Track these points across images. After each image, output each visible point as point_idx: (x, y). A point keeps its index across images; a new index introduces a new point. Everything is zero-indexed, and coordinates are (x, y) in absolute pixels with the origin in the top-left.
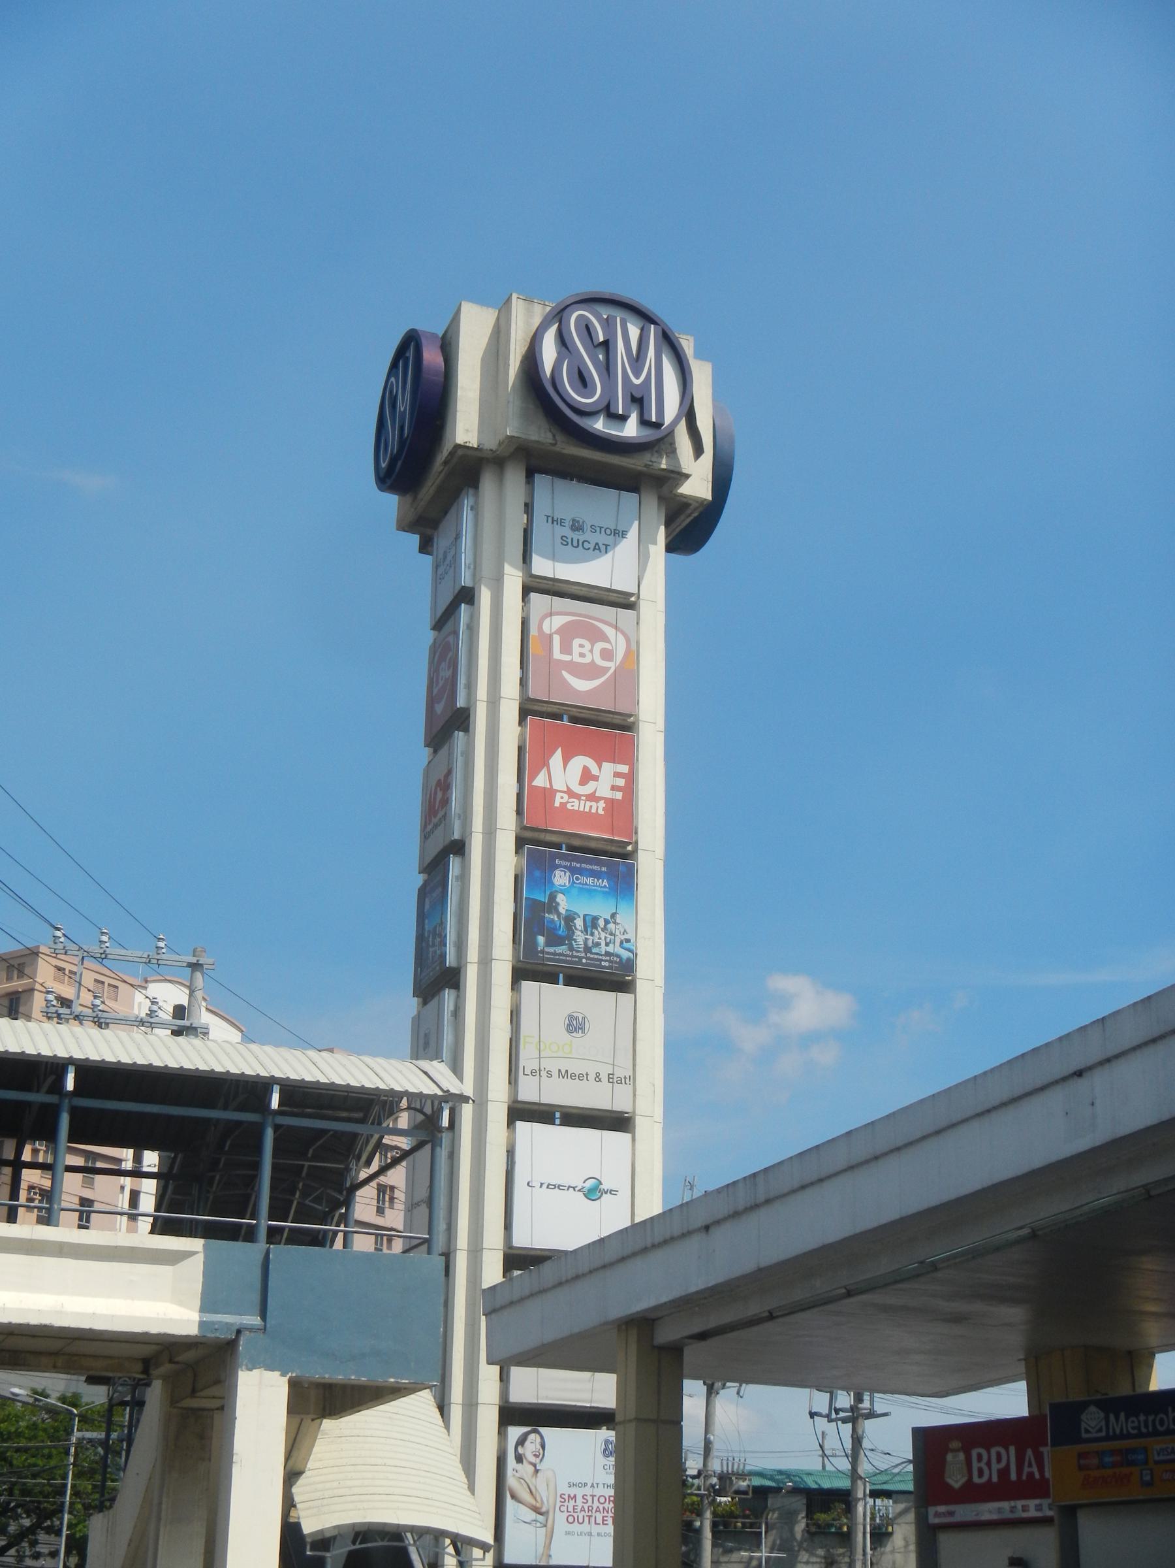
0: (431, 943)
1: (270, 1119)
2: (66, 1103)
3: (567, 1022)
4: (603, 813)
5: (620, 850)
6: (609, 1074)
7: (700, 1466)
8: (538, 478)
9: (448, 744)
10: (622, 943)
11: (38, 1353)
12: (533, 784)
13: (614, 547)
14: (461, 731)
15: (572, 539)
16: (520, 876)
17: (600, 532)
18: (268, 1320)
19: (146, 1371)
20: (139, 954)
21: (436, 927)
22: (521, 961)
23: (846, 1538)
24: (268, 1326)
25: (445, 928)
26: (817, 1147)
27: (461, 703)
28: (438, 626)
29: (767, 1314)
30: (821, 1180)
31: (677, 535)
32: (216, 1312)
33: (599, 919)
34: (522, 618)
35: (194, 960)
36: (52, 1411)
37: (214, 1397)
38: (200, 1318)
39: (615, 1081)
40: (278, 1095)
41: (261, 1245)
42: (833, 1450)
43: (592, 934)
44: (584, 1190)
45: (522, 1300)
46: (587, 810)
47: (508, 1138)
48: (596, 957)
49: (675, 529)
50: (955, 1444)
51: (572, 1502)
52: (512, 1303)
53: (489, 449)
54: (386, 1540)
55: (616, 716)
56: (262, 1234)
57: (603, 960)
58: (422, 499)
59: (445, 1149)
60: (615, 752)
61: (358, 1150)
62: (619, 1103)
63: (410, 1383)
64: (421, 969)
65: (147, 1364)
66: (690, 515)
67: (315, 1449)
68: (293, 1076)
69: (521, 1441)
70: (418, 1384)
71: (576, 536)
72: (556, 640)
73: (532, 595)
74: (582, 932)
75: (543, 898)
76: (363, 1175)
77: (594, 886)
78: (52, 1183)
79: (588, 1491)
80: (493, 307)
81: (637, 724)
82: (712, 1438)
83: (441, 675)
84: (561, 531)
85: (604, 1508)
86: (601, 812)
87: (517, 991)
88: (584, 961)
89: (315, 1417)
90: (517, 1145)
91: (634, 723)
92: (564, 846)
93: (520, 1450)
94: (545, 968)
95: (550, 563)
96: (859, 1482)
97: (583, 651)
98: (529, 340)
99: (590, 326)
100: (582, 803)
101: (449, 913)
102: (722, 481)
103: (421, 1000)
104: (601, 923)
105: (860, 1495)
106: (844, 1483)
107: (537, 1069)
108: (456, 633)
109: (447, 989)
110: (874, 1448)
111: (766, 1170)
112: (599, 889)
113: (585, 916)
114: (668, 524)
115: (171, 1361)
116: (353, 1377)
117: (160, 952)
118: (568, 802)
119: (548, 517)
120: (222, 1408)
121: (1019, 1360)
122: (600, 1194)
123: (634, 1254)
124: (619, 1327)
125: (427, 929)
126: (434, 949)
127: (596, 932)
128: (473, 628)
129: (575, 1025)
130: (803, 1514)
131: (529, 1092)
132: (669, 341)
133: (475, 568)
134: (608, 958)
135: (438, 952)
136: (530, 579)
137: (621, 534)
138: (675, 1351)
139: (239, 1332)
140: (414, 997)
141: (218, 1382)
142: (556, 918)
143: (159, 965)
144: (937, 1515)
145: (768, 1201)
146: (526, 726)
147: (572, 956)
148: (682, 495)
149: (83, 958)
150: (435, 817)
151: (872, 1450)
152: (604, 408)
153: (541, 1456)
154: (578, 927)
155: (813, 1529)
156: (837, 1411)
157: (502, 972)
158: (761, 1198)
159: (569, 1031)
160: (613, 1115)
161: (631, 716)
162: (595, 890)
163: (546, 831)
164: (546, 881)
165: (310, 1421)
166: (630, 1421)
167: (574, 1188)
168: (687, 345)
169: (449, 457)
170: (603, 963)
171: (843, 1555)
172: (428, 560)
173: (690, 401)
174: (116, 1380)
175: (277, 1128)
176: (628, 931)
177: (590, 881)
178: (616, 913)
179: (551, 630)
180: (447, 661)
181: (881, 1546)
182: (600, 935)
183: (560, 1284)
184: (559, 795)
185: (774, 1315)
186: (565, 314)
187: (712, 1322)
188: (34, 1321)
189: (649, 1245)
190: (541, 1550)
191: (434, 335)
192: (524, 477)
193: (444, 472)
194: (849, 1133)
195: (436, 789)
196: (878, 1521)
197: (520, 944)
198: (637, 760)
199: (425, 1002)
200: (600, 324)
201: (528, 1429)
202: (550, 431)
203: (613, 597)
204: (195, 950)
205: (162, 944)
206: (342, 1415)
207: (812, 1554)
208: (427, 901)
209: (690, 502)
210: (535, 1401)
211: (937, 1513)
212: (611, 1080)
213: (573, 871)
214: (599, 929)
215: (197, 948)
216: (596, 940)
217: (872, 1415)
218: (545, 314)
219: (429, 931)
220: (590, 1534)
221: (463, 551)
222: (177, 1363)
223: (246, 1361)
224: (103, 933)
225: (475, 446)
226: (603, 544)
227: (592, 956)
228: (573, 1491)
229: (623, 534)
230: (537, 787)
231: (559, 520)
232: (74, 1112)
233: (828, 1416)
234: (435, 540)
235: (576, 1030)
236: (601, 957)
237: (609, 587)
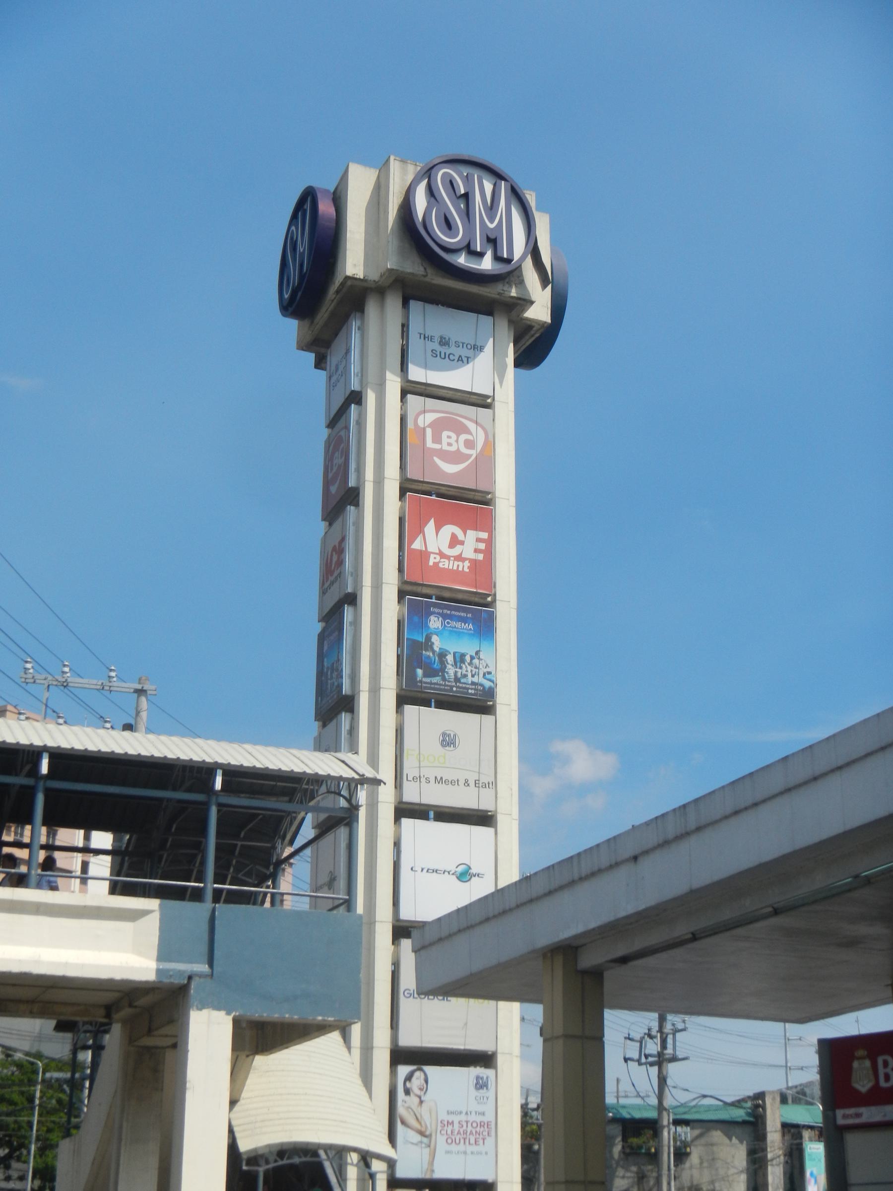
0: (329, 677)
1: (214, 799)
2: (41, 785)
3: (441, 738)
4: (468, 570)
5: (482, 601)
8: (412, 303)
10: (484, 674)
11: (20, 1001)
15: (440, 353)
16: (401, 622)
18: (215, 967)
19: (108, 1015)
20: (95, 682)
21: (333, 664)
22: (403, 689)
23: (654, 1158)
25: (342, 664)
26: (751, 774)
27: (352, 483)
28: (332, 424)
29: (690, 936)
30: (756, 805)
32: (170, 961)
33: (465, 656)
35: (139, 687)
36: (19, 1065)
38: (157, 965)
39: (480, 785)
41: (208, 905)
42: (625, 1092)
43: (461, 668)
45: (450, 936)
48: (464, 686)
49: (520, 348)
50: (861, 1053)
51: (450, 1127)
52: (440, 940)
54: (309, 1156)
56: (209, 895)
59: (344, 842)
61: (283, 831)
62: (485, 804)
64: (321, 699)
65: (109, 1010)
66: (533, 336)
67: (249, 1082)
68: (233, 762)
69: (409, 1078)
71: (444, 350)
72: (429, 432)
73: (409, 396)
74: (452, 666)
75: (421, 638)
76: (288, 851)
77: (461, 629)
78: (30, 854)
79: (463, 1118)
80: (374, 167)
84: (431, 345)
85: (476, 1132)
86: (466, 570)
87: (401, 713)
88: (454, 689)
90: (402, 837)
91: (491, 499)
92: (434, 597)
94: (423, 695)
96: (665, 1114)
97: (450, 441)
98: (404, 193)
99: (454, 182)
100: (451, 562)
102: (558, 309)
103: (321, 723)
104: (468, 658)
105: (665, 1123)
106: (652, 1114)
107: (418, 776)
108: (347, 428)
110: (675, 1085)
111: (696, 801)
113: (454, 654)
115: (130, 1006)
116: (287, 1016)
117: (111, 680)
118: (440, 562)
119: (420, 334)
120: (174, 1046)
121: (887, 985)
122: (469, 877)
123: (561, 888)
124: (544, 956)
126: (332, 681)
127: (464, 666)
129: (448, 741)
130: (619, 1139)
131: (411, 795)
132: (516, 194)
133: (362, 376)
135: (336, 684)
136: (408, 384)
137: (479, 348)
138: (596, 975)
139: (190, 978)
140: (315, 720)
141: (171, 1021)
143: (111, 691)
144: (845, 1117)
145: (699, 829)
146: (405, 501)
147: (445, 685)
148: (527, 319)
149: (49, 686)
152: (465, 247)
153: (425, 1090)
154: (449, 661)
155: (628, 1151)
156: (646, 1056)
157: (388, 698)
158: (692, 825)
161: (489, 493)
162: (463, 632)
163: (423, 585)
164: (423, 625)
166: (557, 1038)
167: (449, 873)
168: (531, 198)
170: (470, 691)
171: (652, 1171)
172: (322, 375)
175: (220, 805)
176: (489, 665)
177: (458, 625)
178: (479, 651)
179: (424, 425)
180: (340, 450)
182: (467, 669)
183: (487, 920)
184: (432, 556)
186: (434, 171)
187: (638, 944)
188: (16, 969)
189: (576, 877)
190: (425, 1166)
191: (327, 191)
192: (401, 306)
193: (335, 301)
194: (785, 759)
195: (332, 556)
196: (678, 1143)
197: (402, 676)
198: (495, 529)
199: (324, 725)
202: (422, 265)
203: (474, 399)
204: (140, 679)
207: (627, 1170)
209: (533, 324)
211: (843, 1117)
213: (445, 617)
214: (466, 664)
215: (141, 678)
216: (464, 672)
217: (674, 1059)
218: (417, 172)
219: (328, 668)
220: (465, 1153)
221: (352, 362)
224: (65, 666)
225: (362, 277)
226: (466, 357)
227: (461, 685)
228: (451, 1118)
229: (481, 349)
231: (430, 337)
232: (48, 792)
235: (448, 745)
236: (468, 686)
237: (470, 391)
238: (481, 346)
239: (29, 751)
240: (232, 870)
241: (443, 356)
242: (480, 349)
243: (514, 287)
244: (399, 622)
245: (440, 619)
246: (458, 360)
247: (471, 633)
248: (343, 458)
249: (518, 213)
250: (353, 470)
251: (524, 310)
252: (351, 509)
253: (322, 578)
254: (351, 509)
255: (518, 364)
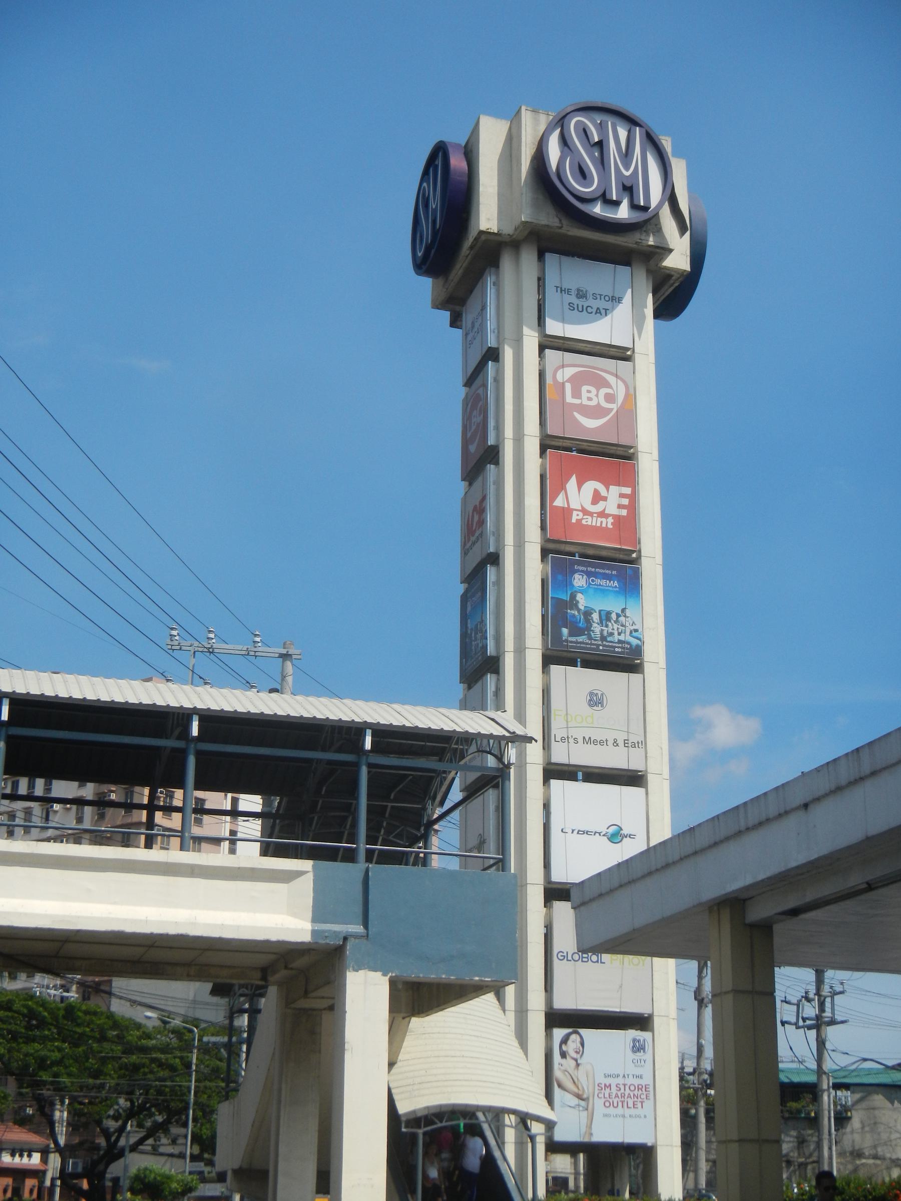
0: (473, 639)
1: (364, 760)
3: (588, 698)
4: (611, 527)
5: (626, 558)
6: (625, 740)
7: (695, 1065)
8: (548, 256)
9: (482, 476)
10: (631, 632)
12: (554, 504)
13: (612, 311)
14: (492, 464)
15: (578, 305)
16: (545, 580)
17: (601, 299)
19: (264, 978)
20: (240, 647)
21: (477, 625)
22: (550, 649)
23: (814, 1122)
24: (370, 933)
25: (486, 625)
27: (491, 441)
28: (469, 382)
31: (661, 303)
33: (611, 613)
34: (539, 370)
35: (284, 651)
37: (323, 998)
39: (630, 745)
40: (370, 738)
43: (607, 626)
44: (608, 834)
45: (612, 891)
46: (598, 525)
47: (544, 793)
48: (610, 644)
51: (608, 1090)
52: (601, 895)
53: (507, 233)
55: (619, 448)
56: (362, 855)
57: (617, 647)
58: (452, 280)
60: (619, 481)
62: (635, 764)
63: (492, 981)
65: (265, 972)
67: (405, 1044)
69: (565, 1041)
70: (499, 981)
71: (581, 302)
72: (568, 387)
73: (547, 351)
75: (565, 597)
76: (438, 812)
77: (606, 586)
79: (620, 1081)
81: (636, 455)
82: (703, 1042)
83: (473, 421)
84: (568, 299)
85: (634, 1095)
86: (610, 526)
88: (601, 648)
89: (405, 1015)
91: (633, 454)
92: (577, 555)
93: (564, 1048)
95: (561, 324)
96: (824, 1077)
97: (590, 395)
100: (595, 519)
101: (488, 612)
102: (698, 257)
104: (614, 616)
105: (825, 1087)
106: (812, 1078)
107: (566, 737)
108: (485, 386)
109: (489, 674)
110: (835, 1049)
111: (870, 744)
112: (611, 589)
113: (600, 611)
114: (655, 292)
115: (286, 967)
116: (444, 976)
117: (256, 645)
118: (582, 519)
120: (331, 1008)
123: (727, 839)
125: (470, 628)
127: (610, 624)
128: (499, 381)
129: (595, 700)
131: (560, 756)
132: (651, 140)
133: (499, 332)
134: (620, 645)
135: (480, 645)
137: (617, 300)
138: (765, 929)
139: (345, 939)
141: (328, 983)
142: (576, 613)
143: (256, 656)
145: (873, 774)
146: (546, 458)
148: (666, 268)
149: (194, 652)
150: (473, 535)
151: (834, 1051)
153: (581, 1053)
154: (595, 620)
155: (787, 1115)
156: (804, 1020)
157: (534, 659)
159: (590, 705)
160: (629, 774)
161: (631, 447)
164: (567, 583)
165: (401, 1019)
166: (726, 993)
167: (600, 834)
168: (667, 144)
169: (475, 242)
170: (617, 650)
171: (812, 1135)
172: (458, 333)
173: (671, 187)
174: (236, 988)
175: (370, 766)
176: (636, 623)
177: (603, 582)
178: (625, 608)
181: (842, 1128)
182: (613, 627)
183: (650, 874)
184: (575, 513)
185: (873, 886)
188: (172, 931)
189: (743, 828)
190: (584, 1129)
193: (470, 256)
197: (548, 635)
200: (594, 126)
201: (570, 1030)
202: (557, 216)
203: (613, 352)
204: (285, 644)
205: (258, 639)
206: (429, 1013)
208: (469, 604)
209: (673, 273)
210: (574, 1007)
212: (626, 745)
213: (589, 574)
214: (612, 622)
216: (610, 631)
217: (833, 1022)
219: (472, 629)
221: (488, 318)
222: (292, 969)
223: (353, 963)
224: (210, 632)
225: (496, 231)
227: (607, 644)
228: (608, 1081)
229: (619, 300)
230: (556, 507)
232: (199, 754)
233: (796, 1025)
234: (464, 315)
235: (596, 704)
236: (614, 645)
238: (619, 298)
239: (179, 713)
240: (383, 831)
241: (580, 309)
242: (619, 300)
243: (651, 235)
244: (543, 581)
245: (585, 577)
246: (596, 313)
247: (617, 591)
248: (482, 416)
249: (654, 158)
250: (492, 428)
251: (662, 259)
252: (491, 468)
253: (463, 540)
254: (491, 468)
255: (657, 315)
